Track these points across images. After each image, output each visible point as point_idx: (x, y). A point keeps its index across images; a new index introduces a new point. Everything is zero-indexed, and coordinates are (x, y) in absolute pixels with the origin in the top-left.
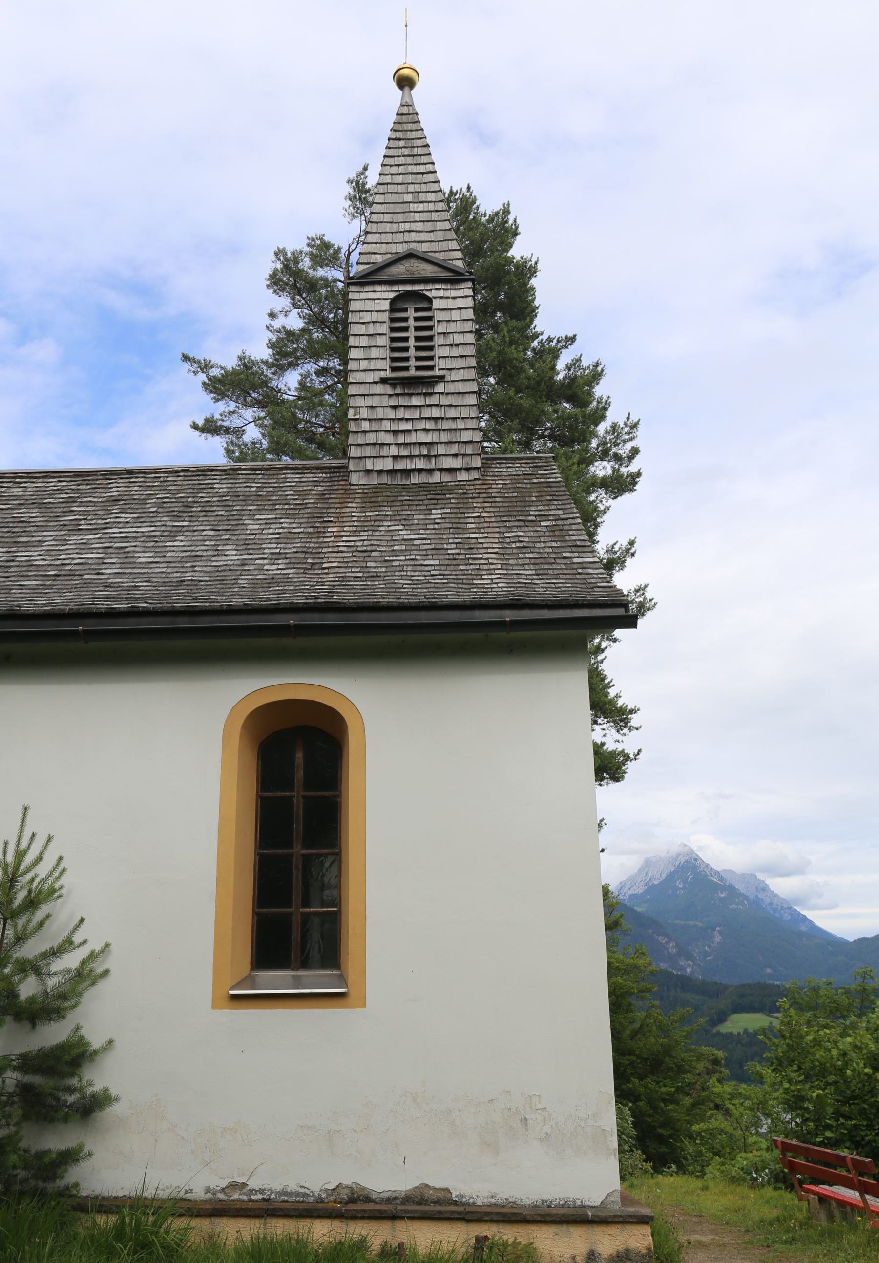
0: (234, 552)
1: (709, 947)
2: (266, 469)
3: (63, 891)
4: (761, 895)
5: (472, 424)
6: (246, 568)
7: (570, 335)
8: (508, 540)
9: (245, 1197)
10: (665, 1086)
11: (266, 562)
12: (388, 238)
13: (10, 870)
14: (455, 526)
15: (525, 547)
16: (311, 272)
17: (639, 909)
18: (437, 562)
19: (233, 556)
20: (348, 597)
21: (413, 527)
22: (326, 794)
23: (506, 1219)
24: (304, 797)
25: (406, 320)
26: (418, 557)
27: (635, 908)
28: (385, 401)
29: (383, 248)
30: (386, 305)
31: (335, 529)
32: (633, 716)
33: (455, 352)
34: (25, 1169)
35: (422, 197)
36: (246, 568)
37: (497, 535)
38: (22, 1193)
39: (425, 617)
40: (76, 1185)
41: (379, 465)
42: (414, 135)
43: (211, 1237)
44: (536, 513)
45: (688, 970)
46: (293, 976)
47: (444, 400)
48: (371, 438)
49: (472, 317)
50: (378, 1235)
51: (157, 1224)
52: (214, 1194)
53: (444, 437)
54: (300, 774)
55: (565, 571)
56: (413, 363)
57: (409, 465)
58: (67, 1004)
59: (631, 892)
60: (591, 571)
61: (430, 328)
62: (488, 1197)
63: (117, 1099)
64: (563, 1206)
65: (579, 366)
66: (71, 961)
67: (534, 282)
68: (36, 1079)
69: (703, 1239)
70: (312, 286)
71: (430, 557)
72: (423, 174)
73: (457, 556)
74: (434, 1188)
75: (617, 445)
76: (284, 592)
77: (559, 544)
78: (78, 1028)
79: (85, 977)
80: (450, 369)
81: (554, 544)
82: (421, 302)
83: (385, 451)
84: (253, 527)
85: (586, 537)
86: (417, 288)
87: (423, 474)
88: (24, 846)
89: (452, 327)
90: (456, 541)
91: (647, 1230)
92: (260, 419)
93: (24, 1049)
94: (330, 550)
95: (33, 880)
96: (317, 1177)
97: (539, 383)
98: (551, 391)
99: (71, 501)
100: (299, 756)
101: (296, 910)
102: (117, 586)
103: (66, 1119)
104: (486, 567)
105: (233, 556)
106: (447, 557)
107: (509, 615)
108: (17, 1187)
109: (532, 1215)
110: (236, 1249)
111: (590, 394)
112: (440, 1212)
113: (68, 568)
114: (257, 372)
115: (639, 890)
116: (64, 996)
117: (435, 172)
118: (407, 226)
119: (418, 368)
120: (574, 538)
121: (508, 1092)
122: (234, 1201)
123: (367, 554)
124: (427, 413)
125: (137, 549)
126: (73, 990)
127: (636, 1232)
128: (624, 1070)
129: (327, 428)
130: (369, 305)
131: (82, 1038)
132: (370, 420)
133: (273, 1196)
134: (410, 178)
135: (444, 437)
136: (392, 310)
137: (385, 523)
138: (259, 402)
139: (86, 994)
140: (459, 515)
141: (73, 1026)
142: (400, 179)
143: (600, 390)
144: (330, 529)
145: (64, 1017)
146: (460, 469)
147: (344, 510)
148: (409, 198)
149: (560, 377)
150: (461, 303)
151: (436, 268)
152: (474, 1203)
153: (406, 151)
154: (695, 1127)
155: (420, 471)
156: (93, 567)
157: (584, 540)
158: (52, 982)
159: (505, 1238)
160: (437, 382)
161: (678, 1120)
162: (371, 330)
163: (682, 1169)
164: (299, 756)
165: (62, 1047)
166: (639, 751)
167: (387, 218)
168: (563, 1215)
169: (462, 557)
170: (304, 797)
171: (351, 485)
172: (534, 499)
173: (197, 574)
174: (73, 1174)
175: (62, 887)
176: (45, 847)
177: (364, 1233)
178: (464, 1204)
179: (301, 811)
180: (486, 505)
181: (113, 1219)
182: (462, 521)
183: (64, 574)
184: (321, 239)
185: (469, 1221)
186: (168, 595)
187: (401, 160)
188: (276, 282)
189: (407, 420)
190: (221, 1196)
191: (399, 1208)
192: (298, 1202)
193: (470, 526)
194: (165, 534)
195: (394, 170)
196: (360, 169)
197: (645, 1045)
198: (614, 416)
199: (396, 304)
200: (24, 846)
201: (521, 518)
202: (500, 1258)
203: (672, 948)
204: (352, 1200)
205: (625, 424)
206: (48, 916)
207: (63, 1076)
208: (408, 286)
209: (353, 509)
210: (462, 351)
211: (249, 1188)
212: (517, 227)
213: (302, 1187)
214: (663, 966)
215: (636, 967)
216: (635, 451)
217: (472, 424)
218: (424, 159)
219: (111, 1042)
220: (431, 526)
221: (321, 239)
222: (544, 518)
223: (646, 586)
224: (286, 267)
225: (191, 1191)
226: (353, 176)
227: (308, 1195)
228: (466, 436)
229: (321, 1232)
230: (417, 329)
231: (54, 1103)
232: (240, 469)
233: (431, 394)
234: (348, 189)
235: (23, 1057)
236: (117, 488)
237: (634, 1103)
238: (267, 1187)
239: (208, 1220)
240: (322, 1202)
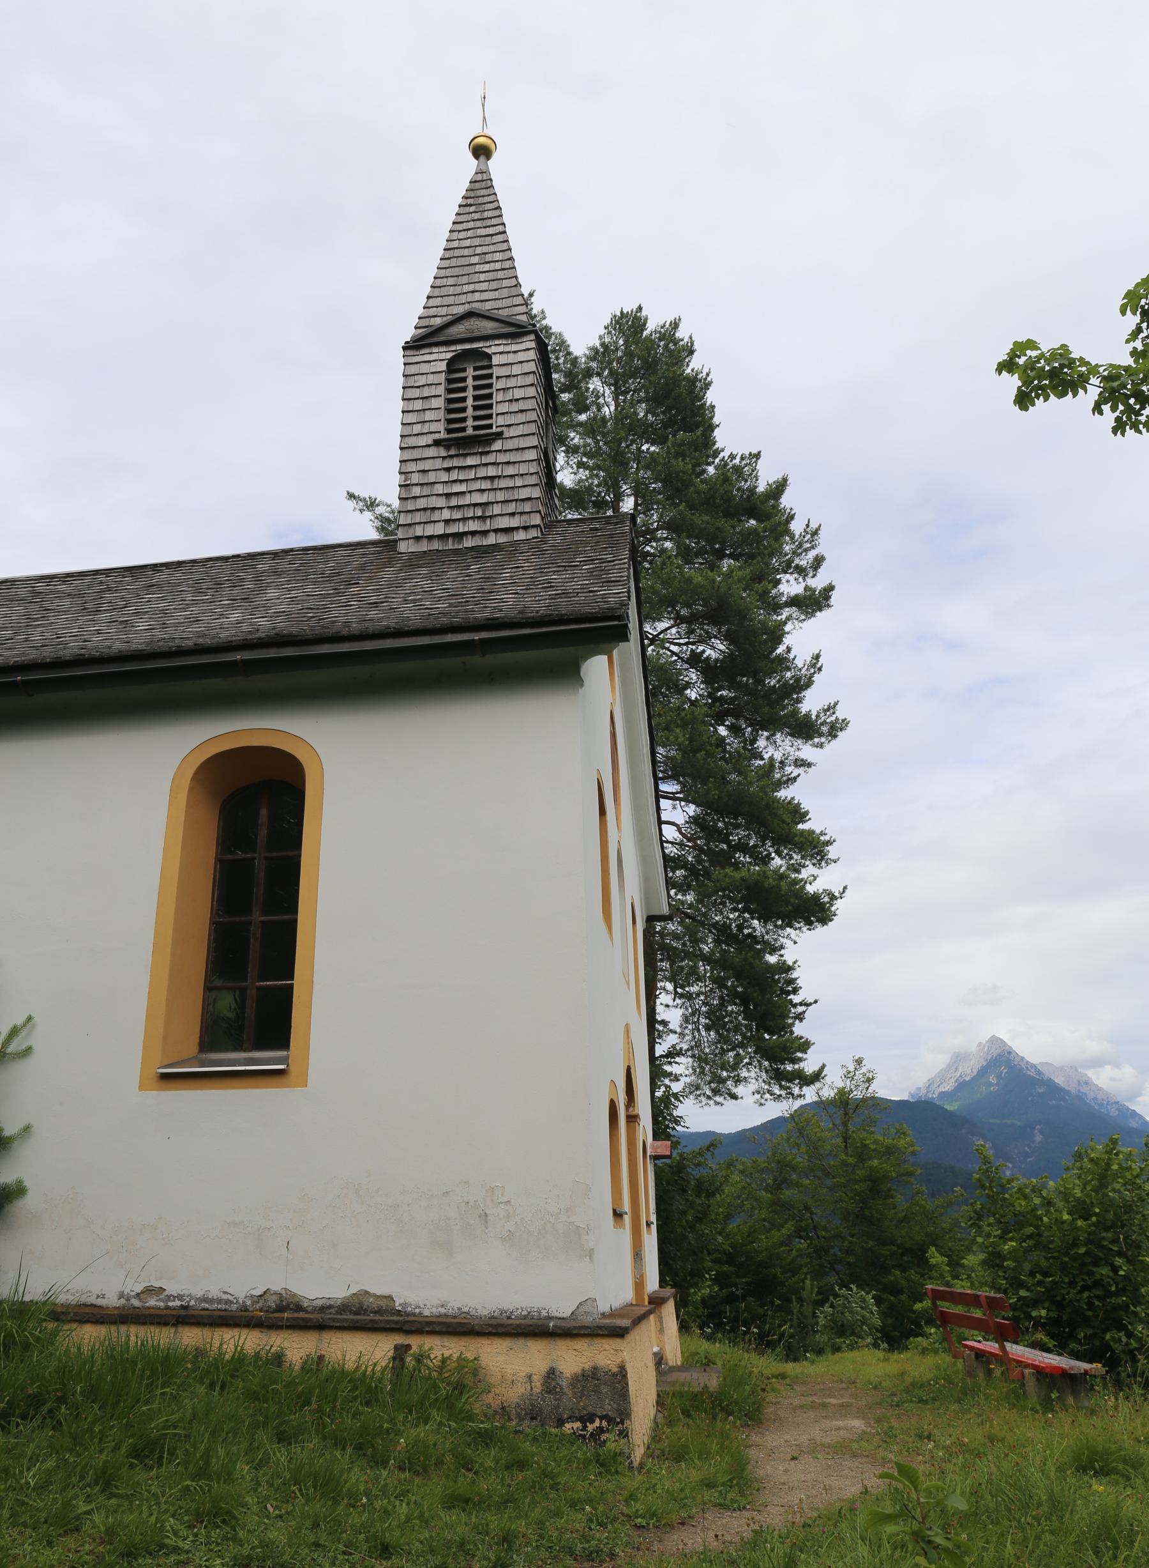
1: (1030, 1147)
4: (1084, 1089)
7: (755, 451)
9: (162, 1304)
12: (451, 300)
17: (949, 1108)
23: (450, 1330)
24: (266, 858)
28: (439, 463)
29: (444, 311)
30: (443, 366)
33: (515, 407)
35: (489, 258)
41: (430, 530)
47: (501, 458)
50: (297, 1348)
52: (128, 1300)
53: (500, 496)
54: (263, 833)
57: (462, 528)
59: (941, 1089)
62: (437, 1307)
64: (525, 1317)
72: (492, 235)
74: (375, 1296)
80: (509, 426)
82: (481, 360)
83: (436, 516)
86: (475, 345)
87: (477, 537)
96: (242, 1281)
100: (264, 813)
109: (481, 1326)
111: (775, 507)
115: (948, 1087)
119: (475, 428)
121: (467, 1183)
122: (149, 1308)
124: (482, 472)
127: (607, 1347)
132: (421, 485)
133: (192, 1303)
134: (477, 241)
135: (500, 496)
142: (467, 243)
146: (517, 528)
148: (475, 260)
150: (522, 356)
151: (496, 324)
152: (420, 1313)
153: (476, 216)
155: (473, 533)
160: (494, 440)
162: (426, 392)
164: (264, 813)
166: (845, 888)
170: (266, 858)
178: (408, 1315)
179: (262, 874)
187: (471, 225)
189: (461, 481)
190: (136, 1302)
192: (220, 1310)
195: (462, 235)
198: (797, 527)
199: (453, 365)
204: (281, 1309)
210: (522, 405)
211: (166, 1293)
212: (692, 344)
213: (225, 1293)
216: (818, 561)
218: (494, 221)
223: (836, 704)
227: (231, 1302)
233: (488, 453)
236: (163, 576)
238: (186, 1292)
240: (247, 1310)
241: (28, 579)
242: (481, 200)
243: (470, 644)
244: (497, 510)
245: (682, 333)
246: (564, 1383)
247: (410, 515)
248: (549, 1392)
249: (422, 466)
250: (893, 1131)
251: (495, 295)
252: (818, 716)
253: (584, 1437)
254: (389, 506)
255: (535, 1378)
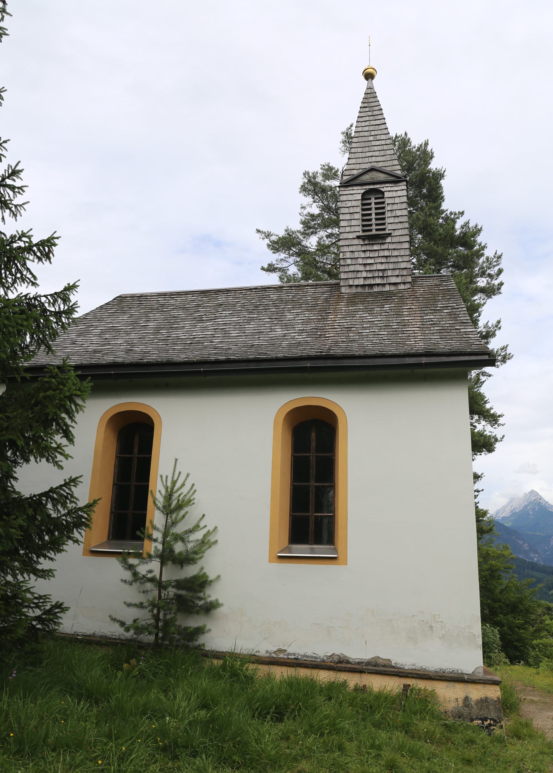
0: (280, 330)
1: (547, 547)
2: (297, 287)
3: (194, 501)
5: (407, 259)
6: (286, 338)
8: (425, 320)
9: (286, 657)
10: (519, 619)
11: (296, 334)
12: (360, 161)
13: (169, 490)
14: (396, 313)
15: (434, 324)
16: (322, 182)
18: (387, 333)
19: (279, 331)
20: (337, 351)
21: (374, 315)
22: (327, 455)
24: (315, 456)
25: (370, 204)
26: (376, 330)
27: (505, 524)
28: (359, 248)
29: (358, 166)
30: (359, 197)
31: (333, 317)
32: (500, 418)
33: (397, 220)
34: (179, 634)
35: (378, 137)
36: (286, 338)
37: (419, 318)
38: (177, 646)
39: (379, 362)
40: (203, 645)
41: (357, 282)
42: (374, 104)
43: (269, 674)
44: (441, 306)
45: (535, 559)
46: (310, 548)
47: (391, 246)
48: (352, 268)
49: (406, 201)
50: (353, 681)
51: (242, 665)
53: (391, 266)
54: (313, 444)
55: (456, 336)
56: (374, 227)
57: (372, 282)
58: (197, 557)
59: (503, 515)
60: (470, 336)
61: (383, 208)
62: (411, 665)
63: (222, 605)
64: (451, 673)
65: (468, 226)
66: (198, 535)
67: (442, 182)
68: (182, 592)
69: (534, 698)
70: (324, 190)
71: (383, 330)
72: (379, 125)
73: (397, 330)
75: (489, 268)
76: (305, 349)
77: (453, 322)
78: (202, 568)
79: (205, 543)
81: (451, 322)
83: (359, 275)
84: (290, 316)
85: (469, 318)
86: (376, 186)
88: (175, 478)
89: (395, 207)
90: (397, 321)
91: (497, 688)
92: (297, 262)
93: (178, 578)
94: (330, 327)
95: (180, 495)
96: (322, 649)
97: (446, 237)
98: (452, 241)
99: (198, 306)
100: (313, 435)
101: (313, 514)
102: (221, 348)
103: (198, 613)
104: (413, 335)
105: (279, 331)
106: (392, 330)
107: (424, 360)
108: (175, 643)
110: (280, 681)
112: (385, 671)
113: (197, 339)
114: (295, 237)
115: (507, 514)
116: (196, 553)
117: (385, 123)
118: (371, 154)
119: (377, 230)
120: (462, 318)
121: (423, 612)
123: (349, 329)
124: (382, 254)
125: (231, 329)
126: (200, 550)
127: (491, 689)
128: (496, 610)
129: (332, 265)
130: (350, 197)
131: (205, 573)
132: (351, 258)
133: (299, 657)
134: (372, 128)
135: (391, 266)
136: (363, 199)
137: (359, 313)
138: (296, 253)
139: (206, 552)
140: (399, 308)
141: (199, 567)
142: (366, 129)
143: (480, 239)
144: (330, 317)
145: (196, 563)
146: (400, 283)
147: (337, 307)
148: (371, 138)
149: (458, 233)
151: (386, 176)
152: (403, 668)
153: (370, 113)
154: (535, 642)
155: (378, 285)
156: (209, 339)
157: (467, 320)
158: (190, 546)
159: (420, 686)
160: (387, 237)
161: (526, 639)
163: (528, 664)
164: (313, 435)
165: (195, 577)
166: (503, 436)
167: (360, 150)
168: (451, 677)
169: (400, 330)
171: (341, 293)
172: (440, 298)
173: (261, 341)
174: (202, 640)
175: (194, 499)
176: (186, 479)
177: (346, 678)
178: (398, 668)
179: (314, 464)
180: (414, 302)
181: (221, 662)
182: (400, 310)
183: (194, 342)
184: (328, 165)
185: (400, 677)
186: (246, 352)
187: (367, 119)
188: (304, 189)
189: (371, 258)
190: (274, 655)
191: (364, 667)
193: (405, 313)
194: (245, 321)
196: (349, 126)
197: (507, 597)
198: (488, 253)
199: (364, 196)
200: (175, 478)
201: (433, 308)
202: (417, 696)
203: (526, 547)
204: (340, 662)
205: (495, 257)
206: (187, 512)
207: (196, 591)
208: (368, 184)
209: (342, 306)
210: (401, 219)
214: (521, 556)
215: (503, 556)
216: (500, 271)
217: (407, 259)
218: (380, 117)
219: (219, 576)
220: (384, 314)
221: (328, 165)
222: (445, 308)
223: (507, 346)
224: (309, 181)
225: (259, 652)
226: (344, 130)
227: (317, 658)
228: (403, 265)
229: (324, 677)
230: (376, 209)
231: (192, 604)
232: (284, 287)
233: (384, 243)
234: (342, 137)
235: (177, 581)
236: (222, 299)
237: (501, 628)
238: (297, 652)
239: (267, 666)
240: (325, 662)
241: (152, 295)
242: (372, 104)
243: (420, 365)
244: (390, 273)
245: (429, 149)
246: (473, 703)
247: (346, 274)
248: (466, 707)
249: (351, 249)
250: (501, 546)
251: (383, 159)
252: (497, 352)
253: (483, 727)
254: (277, 236)
255: (459, 700)
